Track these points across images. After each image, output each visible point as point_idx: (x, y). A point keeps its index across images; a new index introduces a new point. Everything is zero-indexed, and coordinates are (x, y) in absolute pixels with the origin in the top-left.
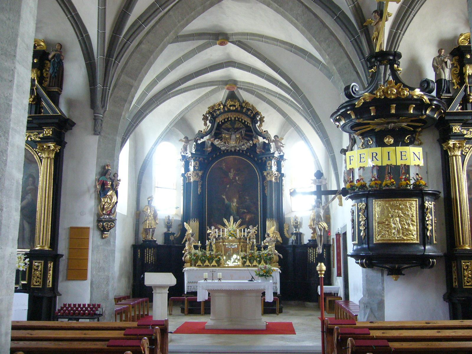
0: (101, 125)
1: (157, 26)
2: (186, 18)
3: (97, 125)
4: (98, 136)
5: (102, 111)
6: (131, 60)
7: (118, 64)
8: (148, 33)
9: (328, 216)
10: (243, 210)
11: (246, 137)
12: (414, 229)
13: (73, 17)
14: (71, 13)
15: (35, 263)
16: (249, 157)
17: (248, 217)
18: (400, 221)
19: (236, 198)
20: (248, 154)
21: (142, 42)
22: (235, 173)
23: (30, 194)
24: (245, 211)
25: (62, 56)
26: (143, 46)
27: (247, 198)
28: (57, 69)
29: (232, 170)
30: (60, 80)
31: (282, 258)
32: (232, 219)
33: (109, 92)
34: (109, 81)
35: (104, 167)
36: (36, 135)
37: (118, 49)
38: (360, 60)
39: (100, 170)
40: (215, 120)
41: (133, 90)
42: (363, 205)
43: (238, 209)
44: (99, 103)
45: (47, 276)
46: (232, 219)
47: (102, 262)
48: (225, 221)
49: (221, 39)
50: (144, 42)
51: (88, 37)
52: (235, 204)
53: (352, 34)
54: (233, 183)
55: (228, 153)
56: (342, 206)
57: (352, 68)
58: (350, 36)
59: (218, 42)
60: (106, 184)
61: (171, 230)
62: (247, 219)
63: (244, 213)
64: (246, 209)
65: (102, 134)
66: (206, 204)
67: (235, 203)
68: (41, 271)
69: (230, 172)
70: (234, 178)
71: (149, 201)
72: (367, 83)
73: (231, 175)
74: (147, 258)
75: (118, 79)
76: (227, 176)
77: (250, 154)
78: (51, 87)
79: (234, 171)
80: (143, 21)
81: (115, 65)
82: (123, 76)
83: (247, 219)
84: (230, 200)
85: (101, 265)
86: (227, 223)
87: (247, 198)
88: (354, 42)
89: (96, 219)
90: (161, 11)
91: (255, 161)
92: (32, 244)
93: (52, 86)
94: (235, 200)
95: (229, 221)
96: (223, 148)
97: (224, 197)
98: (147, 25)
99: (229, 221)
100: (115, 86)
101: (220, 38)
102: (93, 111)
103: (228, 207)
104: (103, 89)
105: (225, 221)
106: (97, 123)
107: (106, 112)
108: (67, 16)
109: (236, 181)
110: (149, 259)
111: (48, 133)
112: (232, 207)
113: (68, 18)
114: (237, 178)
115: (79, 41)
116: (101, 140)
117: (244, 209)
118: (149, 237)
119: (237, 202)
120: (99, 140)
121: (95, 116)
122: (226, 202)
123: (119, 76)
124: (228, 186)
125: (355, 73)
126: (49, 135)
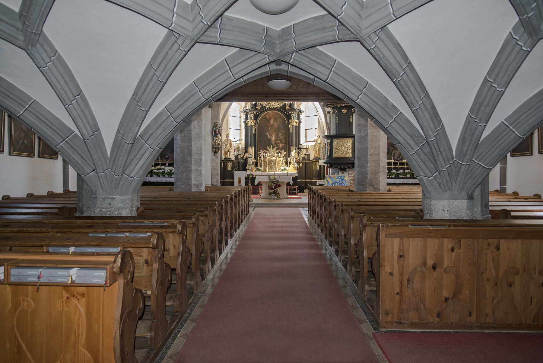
12: (350, 151)
16: (281, 112)
17: (281, 145)
32: (271, 146)
39: (213, 125)
42: (329, 141)
46: (271, 146)
48: (268, 148)
60: (216, 132)
61: (240, 153)
63: (279, 143)
66: (435, 332)
70: (273, 123)
73: (272, 122)
76: (269, 122)
84: (271, 135)
95: (270, 148)
96: (267, 107)
99: (270, 148)
103: (270, 140)
105: (268, 148)
118: (228, 156)
119: (275, 137)
122: (269, 137)
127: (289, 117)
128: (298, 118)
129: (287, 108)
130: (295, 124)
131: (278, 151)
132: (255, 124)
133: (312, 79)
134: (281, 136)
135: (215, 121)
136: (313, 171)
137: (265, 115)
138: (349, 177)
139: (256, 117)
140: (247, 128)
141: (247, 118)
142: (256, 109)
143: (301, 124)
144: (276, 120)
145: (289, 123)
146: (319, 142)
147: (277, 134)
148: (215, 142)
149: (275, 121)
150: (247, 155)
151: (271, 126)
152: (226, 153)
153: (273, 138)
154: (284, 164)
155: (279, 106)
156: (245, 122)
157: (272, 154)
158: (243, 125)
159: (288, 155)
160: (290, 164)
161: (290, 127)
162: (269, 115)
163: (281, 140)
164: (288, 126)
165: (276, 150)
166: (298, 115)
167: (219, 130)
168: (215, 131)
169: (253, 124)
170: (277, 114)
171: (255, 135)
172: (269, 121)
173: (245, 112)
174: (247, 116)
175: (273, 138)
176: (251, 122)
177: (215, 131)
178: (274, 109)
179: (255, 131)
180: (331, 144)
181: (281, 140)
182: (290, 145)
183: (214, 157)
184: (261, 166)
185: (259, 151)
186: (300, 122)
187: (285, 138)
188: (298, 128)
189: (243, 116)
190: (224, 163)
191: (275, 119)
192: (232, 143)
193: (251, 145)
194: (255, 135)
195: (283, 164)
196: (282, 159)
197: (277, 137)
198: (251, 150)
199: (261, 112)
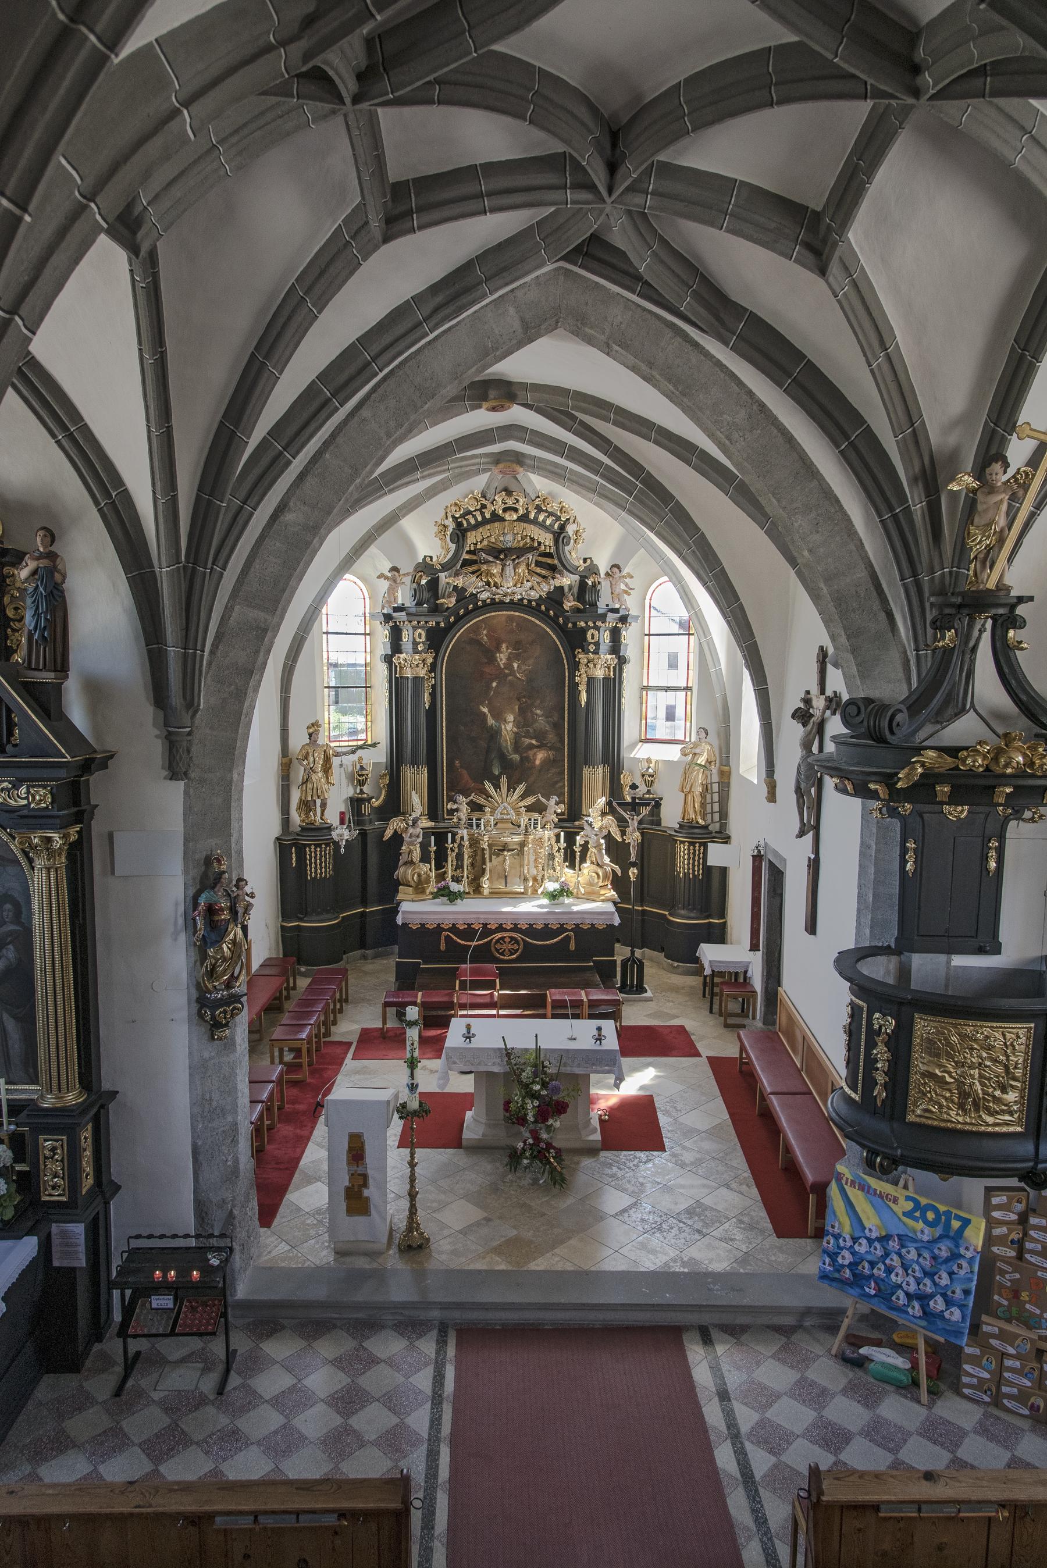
0: (189, 751)
1: (327, 456)
2: (408, 420)
3: (178, 758)
4: (182, 783)
5: (186, 720)
6: (257, 561)
7: (222, 574)
8: (301, 477)
9: (726, 769)
10: (527, 741)
11: (538, 570)
13: (71, 437)
14: (64, 428)
15: (46, 1140)
16: (544, 616)
18: (981, 1076)
19: (513, 713)
20: (543, 608)
21: (285, 506)
22: (511, 653)
23: (11, 947)
24: (534, 742)
25: (59, 572)
26: (289, 517)
27: (538, 712)
28: (46, 619)
29: (504, 646)
30: (59, 649)
31: (620, 874)
33: (202, 656)
34: (203, 615)
35: (208, 861)
36: (8, 790)
37: (222, 523)
38: (902, 580)
39: (196, 872)
40: (464, 536)
41: (269, 634)
43: (517, 737)
44: (176, 698)
45: (81, 1163)
47: (216, 1096)
49: (495, 399)
50: (291, 504)
51: (126, 496)
52: (510, 727)
53: (886, 500)
54: (507, 676)
55: (495, 605)
56: (775, 802)
57: (876, 605)
58: (883, 507)
59: (485, 405)
62: (538, 762)
63: (531, 747)
64: (536, 738)
65: (193, 775)
67: (511, 724)
68: (62, 1161)
69: (501, 652)
70: (509, 666)
71: (310, 735)
72: (913, 647)
73: (502, 658)
74: (311, 873)
75: (224, 619)
77: (547, 610)
78: (35, 669)
79: (507, 648)
80: (283, 444)
81: (216, 576)
82: (237, 608)
83: (538, 762)
84: (499, 716)
85: (214, 1104)
86: (491, 790)
87: (538, 712)
88: (891, 525)
89: (195, 994)
90: (337, 409)
91: (557, 624)
92: (31, 1070)
93: (37, 669)
94: (511, 718)
96: (484, 596)
97: (485, 710)
98: (298, 453)
100: (219, 637)
101: (492, 393)
102: (161, 714)
104: (185, 655)
105: (489, 786)
106: (177, 751)
107: (198, 715)
108: (54, 436)
109: (512, 673)
110: (316, 870)
111: (41, 800)
112: (504, 732)
113: (58, 442)
114: (515, 665)
115: (100, 511)
116: (191, 791)
117: (532, 738)
119: (516, 723)
120: (186, 793)
121: (170, 733)
122: (490, 721)
123: (228, 609)
124: (494, 684)
125: (883, 616)
126: (44, 805)
127: (576, 640)
128: (616, 647)
129: (569, 604)
130: (600, 673)
131: (530, 800)
132: (433, 668)
133: (398, 90)
134: (541, 719)
135: (209, 844)
136: (674, 877)
137: (476, 628)
138: (991, 1223)
139: (436, 639)
140: (397, 684)
141: (396, 646)
142: (435, 609)
143: (626, 668)
144: (519, 649)
145: (575, 666)
146: (702, 760)
147: (523, 711)
148: (212, 973)
149: (517, 657)
150: (396, 824)
151: (501, 676)
152: (306, 806)
153: (509, 727)
154: (559, 857)
155: (534, 595)
156: (388, 659)
157: (509, 818)
158: (381, 671)
159: (572, 819)
160: (583, 860)
161: (581, 680)
162: (492, 630)
163: (540, 736)
164: (572, 676)
165: (523, 797)
166: (615, 633)
167: (234, 901)
168: (211, 911)
169: (422, 672)
170: (523, 625)
171: (432, 714)
172: (489, 654)
173: (388, 618)
174: (396, 634)
175: (509, 727)
176: (414, 663)
177: (211, 911)
178: (517, 605)
179: (433, 695)
180: (900, 1044)
181: (540, 736)
182: (579, 759)
183: (209, 1051)
184: (457, 880)
185: (451, 799)
186: (622, 661)
187: (557, 727)
188: (613, 686)
189: (383, 634)
190: (301, 850)
191: (517, 645)
192: (335, 761)
193: (415, 762)
194: (432, 714)
195: (551, 857)
196: (547, 835)
197: (524, 721)
198: (415, 783)
199: (459, 618)
